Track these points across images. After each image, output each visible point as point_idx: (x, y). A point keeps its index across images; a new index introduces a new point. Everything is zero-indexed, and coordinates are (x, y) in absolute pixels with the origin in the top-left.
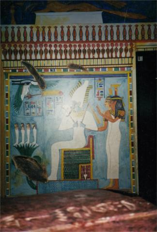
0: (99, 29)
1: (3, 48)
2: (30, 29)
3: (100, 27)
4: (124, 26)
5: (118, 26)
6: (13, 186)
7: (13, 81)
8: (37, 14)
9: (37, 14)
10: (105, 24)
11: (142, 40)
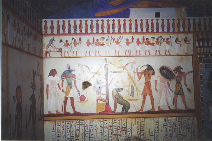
0: (68, 23)
1: (197, 37)
2: (96, 22)
3: (152, 20)
4: (205, 19)
5: (86, 21)
6: (91, 93)
7: (206, 65)
8: (131, 9)
9: (131, 9)
10: (156, 18)
11: (156, 32)
